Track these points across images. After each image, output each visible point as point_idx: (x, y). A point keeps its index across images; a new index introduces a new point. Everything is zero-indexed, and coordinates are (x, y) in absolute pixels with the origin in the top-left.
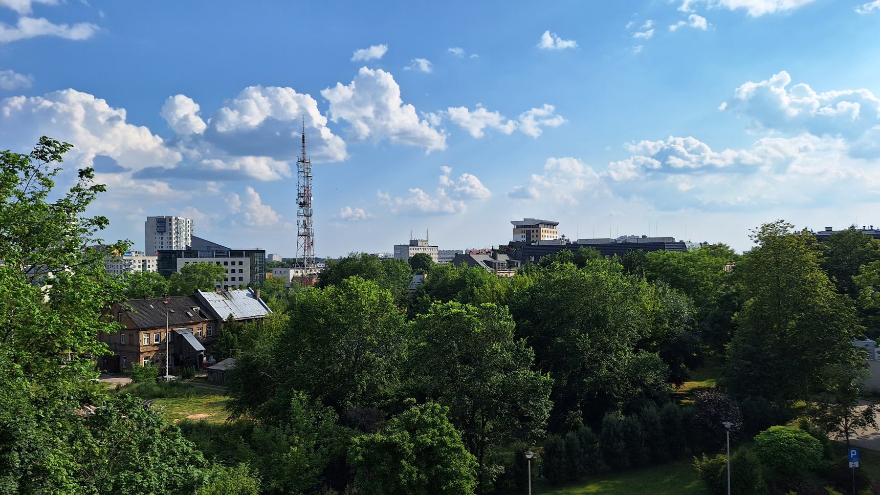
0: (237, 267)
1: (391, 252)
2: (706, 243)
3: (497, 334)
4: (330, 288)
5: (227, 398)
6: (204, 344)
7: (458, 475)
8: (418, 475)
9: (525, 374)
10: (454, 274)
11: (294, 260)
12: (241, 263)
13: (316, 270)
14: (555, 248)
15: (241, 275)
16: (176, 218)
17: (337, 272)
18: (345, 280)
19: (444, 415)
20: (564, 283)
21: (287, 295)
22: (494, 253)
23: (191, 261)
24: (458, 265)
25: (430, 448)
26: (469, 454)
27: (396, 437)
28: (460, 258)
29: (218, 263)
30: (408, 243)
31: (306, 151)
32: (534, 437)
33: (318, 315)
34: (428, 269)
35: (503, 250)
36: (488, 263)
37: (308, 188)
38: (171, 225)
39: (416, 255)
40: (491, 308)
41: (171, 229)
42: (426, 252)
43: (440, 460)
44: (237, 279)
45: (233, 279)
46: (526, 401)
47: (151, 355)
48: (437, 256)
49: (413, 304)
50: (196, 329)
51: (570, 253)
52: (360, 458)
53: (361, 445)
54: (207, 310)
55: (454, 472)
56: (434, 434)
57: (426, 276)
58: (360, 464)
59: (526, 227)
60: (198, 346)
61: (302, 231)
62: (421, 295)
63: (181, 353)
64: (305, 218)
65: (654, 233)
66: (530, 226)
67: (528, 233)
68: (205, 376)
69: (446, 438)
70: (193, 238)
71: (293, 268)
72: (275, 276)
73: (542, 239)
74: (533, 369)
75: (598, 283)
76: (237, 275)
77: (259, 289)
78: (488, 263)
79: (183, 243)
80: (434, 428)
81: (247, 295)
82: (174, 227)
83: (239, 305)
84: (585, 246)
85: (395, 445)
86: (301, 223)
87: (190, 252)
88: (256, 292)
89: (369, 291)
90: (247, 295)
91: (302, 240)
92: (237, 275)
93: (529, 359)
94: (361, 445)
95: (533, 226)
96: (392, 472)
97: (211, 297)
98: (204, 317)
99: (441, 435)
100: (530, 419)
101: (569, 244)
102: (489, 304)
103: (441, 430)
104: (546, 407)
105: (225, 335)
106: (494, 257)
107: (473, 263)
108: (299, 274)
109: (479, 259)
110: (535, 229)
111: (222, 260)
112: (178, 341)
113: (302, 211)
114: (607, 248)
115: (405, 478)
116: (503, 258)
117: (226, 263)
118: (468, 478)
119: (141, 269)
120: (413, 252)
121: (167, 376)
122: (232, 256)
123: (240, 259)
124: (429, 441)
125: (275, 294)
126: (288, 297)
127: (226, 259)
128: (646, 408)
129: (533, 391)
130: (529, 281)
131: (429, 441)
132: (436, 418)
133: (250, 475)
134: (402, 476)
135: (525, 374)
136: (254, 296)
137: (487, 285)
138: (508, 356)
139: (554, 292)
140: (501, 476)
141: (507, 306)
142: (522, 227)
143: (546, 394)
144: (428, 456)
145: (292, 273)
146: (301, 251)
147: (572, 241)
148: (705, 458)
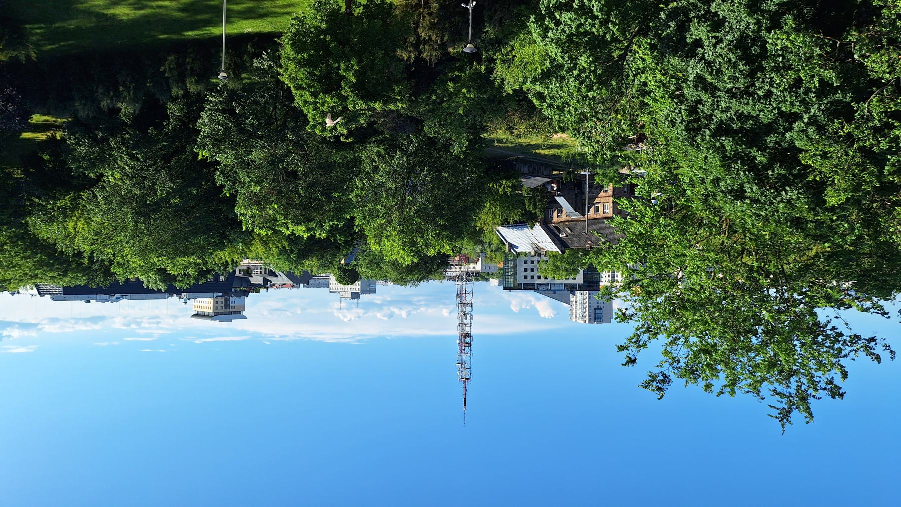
0: (529, 274)
1: (380, 285)
2: (13, 294)
3: (259, 201)
4: (432, 252)
5: (537, 151)
6: (556, 201)
7: (301, 63)
8: (339, 66)
9: (226, 158)
10: (311, 264)
11: (477, 280)
12: (525, 277)
13: (454, 271)
14: (196, 290)
15: (525, 266)
16: (585, 322)
17: (428, 267)
18: (416, 261)
19: (312, 123)
20: (183, 254)
21: (482, 245)
22: (266, 284)
23: (571, 281)
24: (306, 272)
25: (326, 92)
26: (287, 82)
27: (361, 105)
28: (306, 279)
29: (546, 278)
30: (362, 296)
31: (462, 390)
32: (220, 93)
33: (444, 227)
34: (340, 268)
35: (256, 288)
36: (273, 274)
37: (462, 351)
38: (590, 316)
39: (353, 283)
40: (261, 228)
41: (590, 311)
42: (342, 286)
43: (320, 79)
44: (529, 262)
45: (532, 262)
46: (227, 129)
47: (602, 193)
48: (331, 282)
49: (352, 237)
50: (563, 217)
51: (177, 285)
52: (397, 89)
53: (396, 100)
54: (553, 234)
55: (303, 66)
56: (323, 105)
57: (343, 262)
58: (398, 82)
59: (230, 313)
60: (561, 200)
61: (468, 309)
62: (346, 242)
63: (576, 195)
64: (465, 321)
65: (77, 307)
66: (225, 313)
67: (227, 305)
68: (554, 172)
69: (310, 99)
70: (568, 302)
71: (478, 272)
72: (494, 264)
73: (211, 300)
74: (218, 163)
75: (143, 252)
76: (529, 266)
77: (506, 250)
78: (273, 274)
79: (580, 298)
80: (323, 111)
81: (517, 247)
82: (587, 313)
83: (529, 239)
84: (159, 291)
85: (362, 98)
86: (468, 317)
87: (572, 289)
88: (509, 250)
89: (394, 249)
90: (517, 247)
91: (468, 300)
92: (529, 266)
93: (222, 172)
94: (396, 100)
95: (222, 314)
96: (365, 72)
97: (550, 246)
98: (556, 227)
99: (316, 103)
100: (223, 111)
101: (179, 293)
102: (263, 232)
103: (315, 109)
104: (205, 123)
105: (533, 211)
106: (266, 281)
107: (290, 275)
108: (471, 265)
109: (283, 279)
110: (220, 310)
111: (542, 281)
112: (579, 207)
113: (468, 329)
114: (134, 289)
115: (353, 66)
116: (256, 279)
117: (539, 278)
118: (289, 59)
119: (616, 274)
120: (357, 287)
121: (587, 173)
122: (534, 285)
123: (526, 281)
124: (328, 99)
125: (494, 247)
126: (480, 242)
127: (539, 281)
128: (91, 115)
129: (217, 141)
130: (225, 255)
131: (328, 99)
132: (320, 120)
133: (503, 80)
134: (356, 67)
135: (226, 158)
136: (511, 246)
137: (275, 250)
138: (243, 176)
139: (199, 242)
140: (258, 55)
141: (244, 229)
142: (235, 313)
143: (205, 136)
144: (329, 83)
145: (478, 267)
146: (469, 289)
147: (175, 297)
148: (22, 58)
